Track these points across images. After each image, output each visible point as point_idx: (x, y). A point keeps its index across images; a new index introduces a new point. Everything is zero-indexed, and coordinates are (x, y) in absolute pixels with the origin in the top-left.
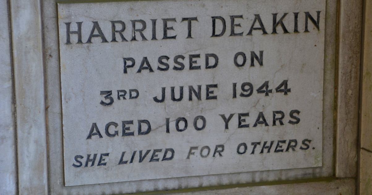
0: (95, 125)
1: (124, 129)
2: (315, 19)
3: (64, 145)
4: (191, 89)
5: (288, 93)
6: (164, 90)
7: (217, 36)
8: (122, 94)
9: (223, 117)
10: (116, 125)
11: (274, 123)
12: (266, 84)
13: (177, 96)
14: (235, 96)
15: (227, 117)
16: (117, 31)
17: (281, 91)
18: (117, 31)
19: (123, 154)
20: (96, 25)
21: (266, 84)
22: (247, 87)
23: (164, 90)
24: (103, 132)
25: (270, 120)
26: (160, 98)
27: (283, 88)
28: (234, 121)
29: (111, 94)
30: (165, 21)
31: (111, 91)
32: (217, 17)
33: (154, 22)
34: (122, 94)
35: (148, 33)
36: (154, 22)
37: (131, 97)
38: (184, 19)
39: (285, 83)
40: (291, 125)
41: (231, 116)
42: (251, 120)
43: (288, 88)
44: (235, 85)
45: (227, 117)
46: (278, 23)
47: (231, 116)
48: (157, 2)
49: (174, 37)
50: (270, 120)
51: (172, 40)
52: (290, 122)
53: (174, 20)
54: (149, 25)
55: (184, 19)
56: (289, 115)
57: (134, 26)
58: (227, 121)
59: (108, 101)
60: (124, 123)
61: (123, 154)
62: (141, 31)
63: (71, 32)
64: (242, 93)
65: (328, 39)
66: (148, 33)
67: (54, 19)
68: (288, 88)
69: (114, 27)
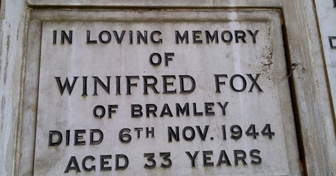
3: (55, 4)
5: (273, 137)
9: (188, 153)
10: (93, 158)
11: (236, 163)
12: (253, 127)
21: (253, 127)
22: (236, 130)
25: (232, 159)
28: (200, 160)
30: (129, 78)
32: (187, 76)
36: (85, 79)
39: (268, 126)
41: (197, 153)
42: (215, 159)
44: (224, 127)
48: (156, 69)
50: (232, 159)
51: (215, 89)
58: (193, 159)
60: (103, 157)
63: (167, 83)
64: (232, 135)
67: (292, 62)
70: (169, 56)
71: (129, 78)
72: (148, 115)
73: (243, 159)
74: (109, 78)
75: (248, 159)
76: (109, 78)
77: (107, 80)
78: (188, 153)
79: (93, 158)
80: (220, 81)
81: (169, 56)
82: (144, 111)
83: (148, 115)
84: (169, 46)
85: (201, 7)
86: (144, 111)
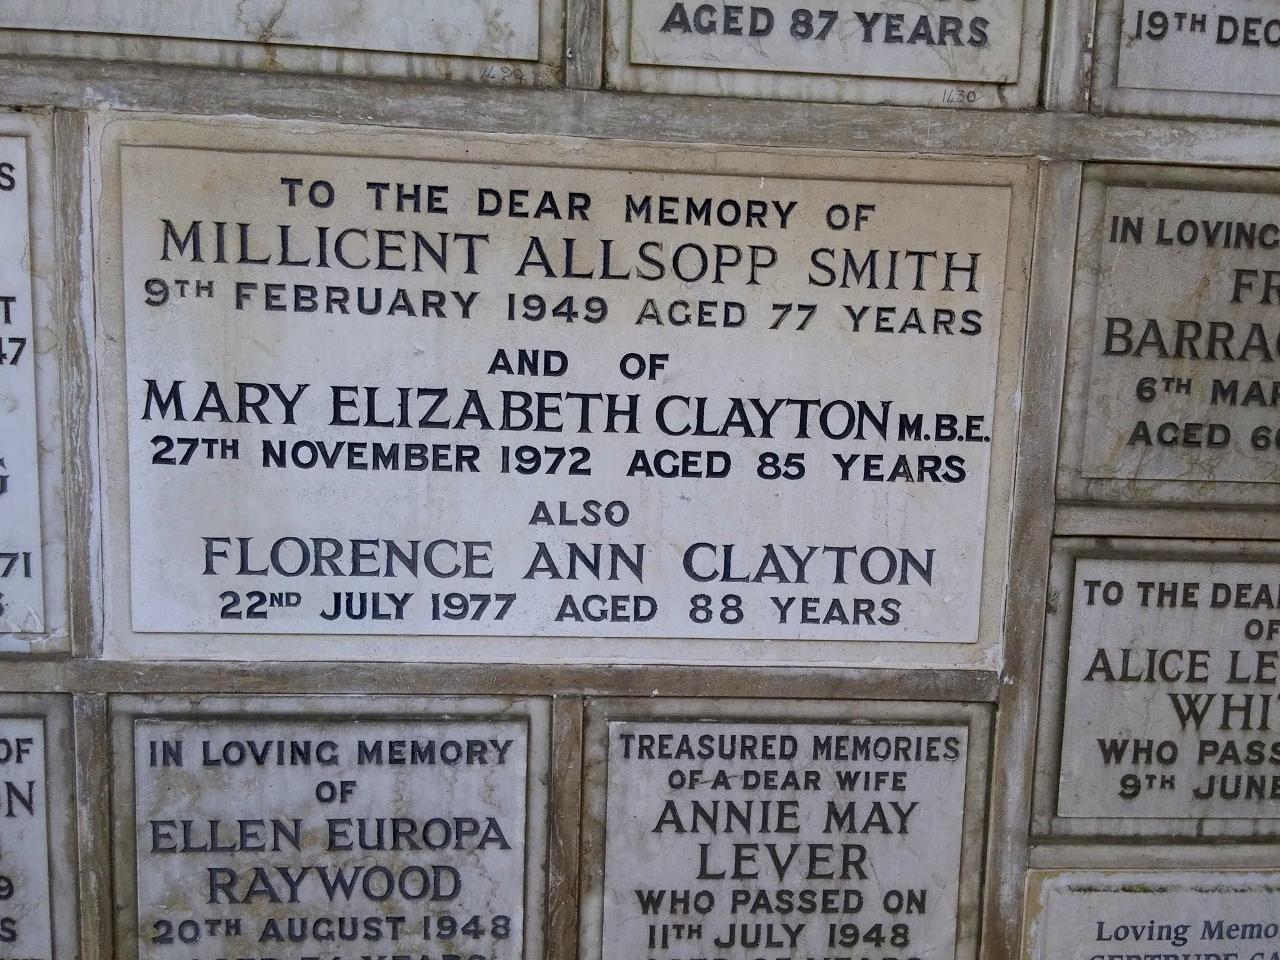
2: (711, 814)
9: (776, 600)
10: (685, 304)
15: (400, 597)
16: (249, 405)
17: (873, 940)
18: (249, 405)
19: (500, 616)
20: (212, 387)
27: (874, 935)
35: (912, 753)
40: (965, 336)
43: (574, 310)
45: (400, 597)
46: (1189, 715)
52: (963, 331)
56: (960, 315)
57: (242, 394)
58: (846, 467)
61: (500, 616)
65: (968, 840)
66: (912, 753)
68: (574, 310)
69: (242, 394)
70: (347, 788)
71: (431, 189)
72: (329, 309)
73: (955, 34)
74: (597, 547)
75: (965, 34)
76: (597, 547)
77: (426, 397)
78: (776, 600)
79: (685, 304)
80: (666, 208)
81: (347, 788)
82: (321, 299)
83: (329, 309)
84: (347, 768)
85: (339, 715)
86: (321, 299)
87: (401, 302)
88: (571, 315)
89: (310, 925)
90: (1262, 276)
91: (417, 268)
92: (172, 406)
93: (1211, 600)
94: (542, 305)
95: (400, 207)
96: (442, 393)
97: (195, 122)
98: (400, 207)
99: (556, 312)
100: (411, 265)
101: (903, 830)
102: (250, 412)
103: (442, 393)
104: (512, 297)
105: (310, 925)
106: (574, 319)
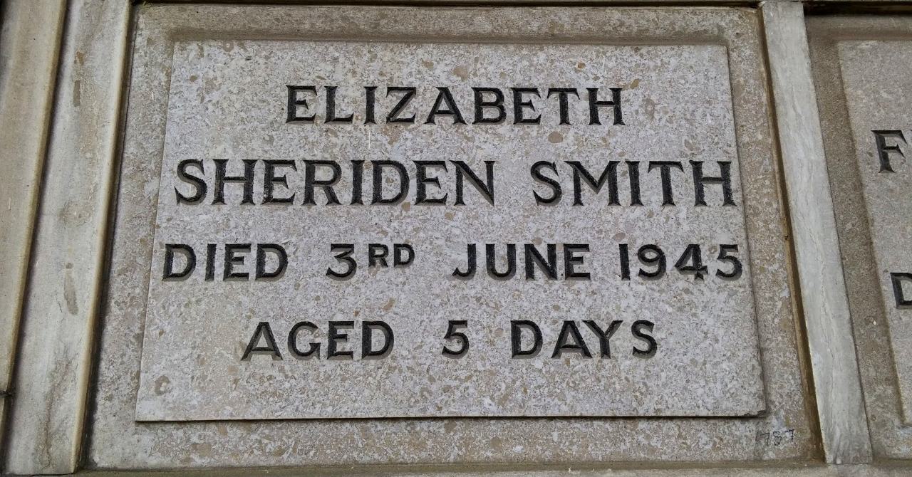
0: (264, 327)
1: (334, 337)
4: (530, 249)
6: (472, 249)
7: (176, 276)
8: (376, 255)
13: (501, 267)
14: (626, 275)
23: (472, 249)
24: (283, 346)
26: (464, 268)
29: (352, 251)
31: (351, 246)
33: (212, 248)
34: (376, 255)
37: (398, 262)
38: (551, 91)
47: (615, 325)
49: (536, 121)
53: (535, 90)
54: (347, 173)
55: (551, 91)
59: (342, 268)
60: (333, 325)
62: (327, 186)
87: (444, 106)
88: (699, 271)
89: (201, 269)
90: (302, 167)
91: (459, 201)
92: (605, 188)
93: (571, 242)
94: (661, 259)
95: (594, 120)
96: (411, 92)
97: (826, 394)
98: (594, 120)
99: (680, 266)
100: (452, 198)
101: (605, 352)
102: (319, 192)
103: (411, 92)
104: (624, 248)
105: (201, 269)
106: (705, 276)
